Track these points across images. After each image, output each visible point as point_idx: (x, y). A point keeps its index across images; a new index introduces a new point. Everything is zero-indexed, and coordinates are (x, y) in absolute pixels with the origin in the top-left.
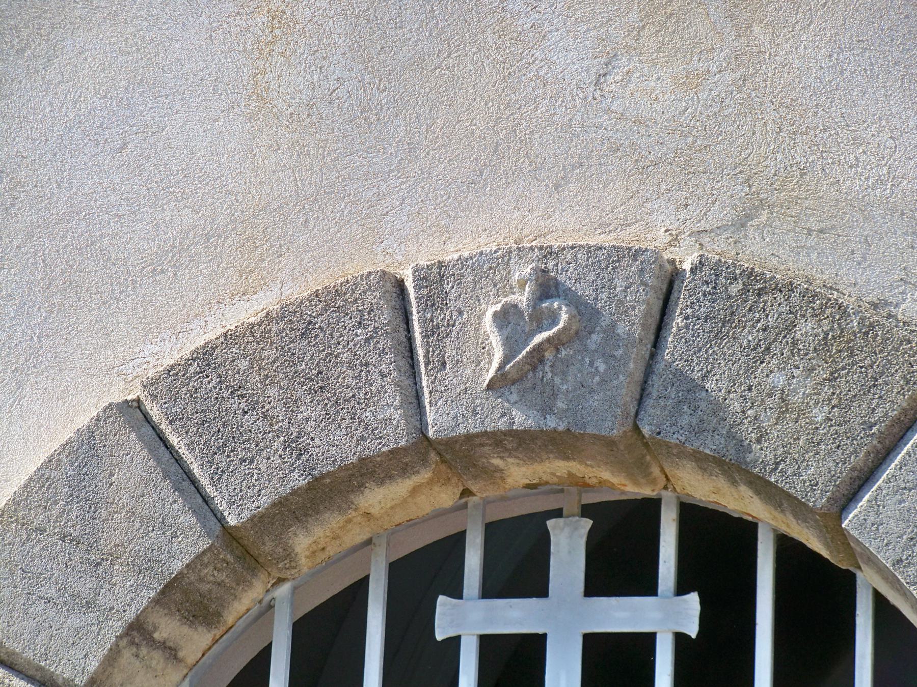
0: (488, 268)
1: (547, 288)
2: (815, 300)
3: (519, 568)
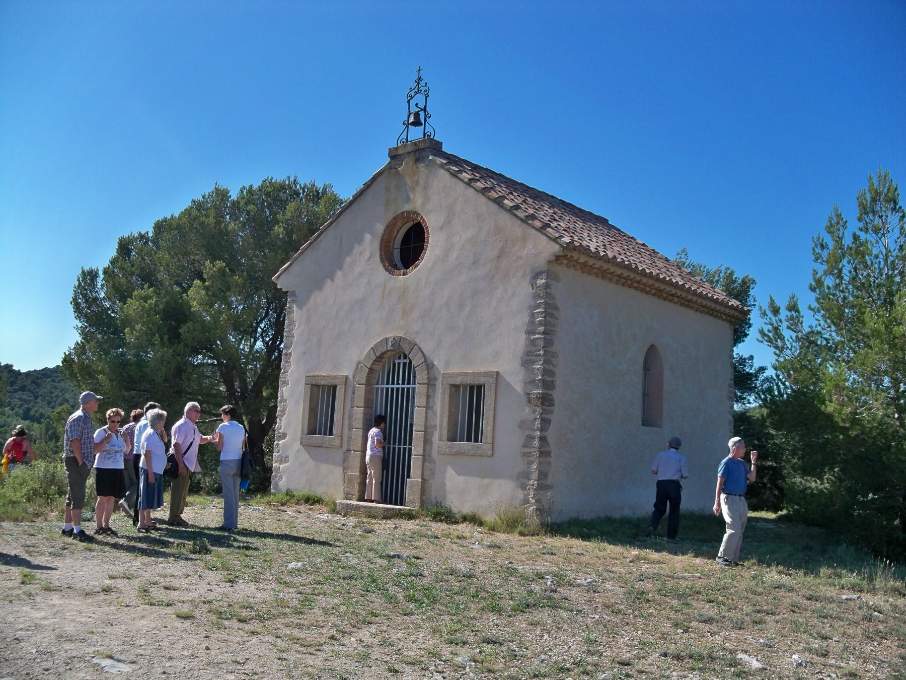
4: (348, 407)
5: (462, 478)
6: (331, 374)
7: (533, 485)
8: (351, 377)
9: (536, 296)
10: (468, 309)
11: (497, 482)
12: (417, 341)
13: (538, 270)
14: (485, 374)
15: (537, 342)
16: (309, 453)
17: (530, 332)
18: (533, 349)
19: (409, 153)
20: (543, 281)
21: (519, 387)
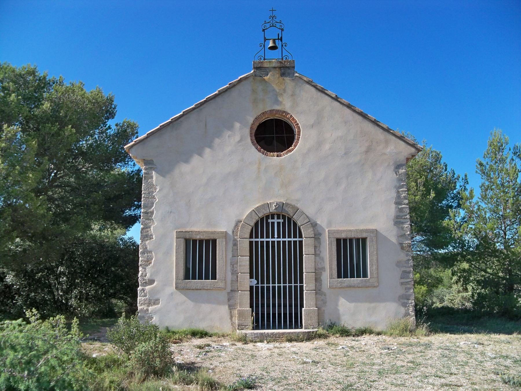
0: (273, 203)
3: (273, 218)
4: (230, 255)
6: (206, 229)
7: (411, 303)
8: (230, 233)
9: (400, 180)
10: (343, 186)
11: (382, 305)
12: (298, 205)
13: (398, 163)
14: (367, 231)
15: (404, 210)
16: (185, 295)
17: (397, 203)
18: (401, 214)
19: (275, 68)
20: (404, 170)
21: (394, 240)
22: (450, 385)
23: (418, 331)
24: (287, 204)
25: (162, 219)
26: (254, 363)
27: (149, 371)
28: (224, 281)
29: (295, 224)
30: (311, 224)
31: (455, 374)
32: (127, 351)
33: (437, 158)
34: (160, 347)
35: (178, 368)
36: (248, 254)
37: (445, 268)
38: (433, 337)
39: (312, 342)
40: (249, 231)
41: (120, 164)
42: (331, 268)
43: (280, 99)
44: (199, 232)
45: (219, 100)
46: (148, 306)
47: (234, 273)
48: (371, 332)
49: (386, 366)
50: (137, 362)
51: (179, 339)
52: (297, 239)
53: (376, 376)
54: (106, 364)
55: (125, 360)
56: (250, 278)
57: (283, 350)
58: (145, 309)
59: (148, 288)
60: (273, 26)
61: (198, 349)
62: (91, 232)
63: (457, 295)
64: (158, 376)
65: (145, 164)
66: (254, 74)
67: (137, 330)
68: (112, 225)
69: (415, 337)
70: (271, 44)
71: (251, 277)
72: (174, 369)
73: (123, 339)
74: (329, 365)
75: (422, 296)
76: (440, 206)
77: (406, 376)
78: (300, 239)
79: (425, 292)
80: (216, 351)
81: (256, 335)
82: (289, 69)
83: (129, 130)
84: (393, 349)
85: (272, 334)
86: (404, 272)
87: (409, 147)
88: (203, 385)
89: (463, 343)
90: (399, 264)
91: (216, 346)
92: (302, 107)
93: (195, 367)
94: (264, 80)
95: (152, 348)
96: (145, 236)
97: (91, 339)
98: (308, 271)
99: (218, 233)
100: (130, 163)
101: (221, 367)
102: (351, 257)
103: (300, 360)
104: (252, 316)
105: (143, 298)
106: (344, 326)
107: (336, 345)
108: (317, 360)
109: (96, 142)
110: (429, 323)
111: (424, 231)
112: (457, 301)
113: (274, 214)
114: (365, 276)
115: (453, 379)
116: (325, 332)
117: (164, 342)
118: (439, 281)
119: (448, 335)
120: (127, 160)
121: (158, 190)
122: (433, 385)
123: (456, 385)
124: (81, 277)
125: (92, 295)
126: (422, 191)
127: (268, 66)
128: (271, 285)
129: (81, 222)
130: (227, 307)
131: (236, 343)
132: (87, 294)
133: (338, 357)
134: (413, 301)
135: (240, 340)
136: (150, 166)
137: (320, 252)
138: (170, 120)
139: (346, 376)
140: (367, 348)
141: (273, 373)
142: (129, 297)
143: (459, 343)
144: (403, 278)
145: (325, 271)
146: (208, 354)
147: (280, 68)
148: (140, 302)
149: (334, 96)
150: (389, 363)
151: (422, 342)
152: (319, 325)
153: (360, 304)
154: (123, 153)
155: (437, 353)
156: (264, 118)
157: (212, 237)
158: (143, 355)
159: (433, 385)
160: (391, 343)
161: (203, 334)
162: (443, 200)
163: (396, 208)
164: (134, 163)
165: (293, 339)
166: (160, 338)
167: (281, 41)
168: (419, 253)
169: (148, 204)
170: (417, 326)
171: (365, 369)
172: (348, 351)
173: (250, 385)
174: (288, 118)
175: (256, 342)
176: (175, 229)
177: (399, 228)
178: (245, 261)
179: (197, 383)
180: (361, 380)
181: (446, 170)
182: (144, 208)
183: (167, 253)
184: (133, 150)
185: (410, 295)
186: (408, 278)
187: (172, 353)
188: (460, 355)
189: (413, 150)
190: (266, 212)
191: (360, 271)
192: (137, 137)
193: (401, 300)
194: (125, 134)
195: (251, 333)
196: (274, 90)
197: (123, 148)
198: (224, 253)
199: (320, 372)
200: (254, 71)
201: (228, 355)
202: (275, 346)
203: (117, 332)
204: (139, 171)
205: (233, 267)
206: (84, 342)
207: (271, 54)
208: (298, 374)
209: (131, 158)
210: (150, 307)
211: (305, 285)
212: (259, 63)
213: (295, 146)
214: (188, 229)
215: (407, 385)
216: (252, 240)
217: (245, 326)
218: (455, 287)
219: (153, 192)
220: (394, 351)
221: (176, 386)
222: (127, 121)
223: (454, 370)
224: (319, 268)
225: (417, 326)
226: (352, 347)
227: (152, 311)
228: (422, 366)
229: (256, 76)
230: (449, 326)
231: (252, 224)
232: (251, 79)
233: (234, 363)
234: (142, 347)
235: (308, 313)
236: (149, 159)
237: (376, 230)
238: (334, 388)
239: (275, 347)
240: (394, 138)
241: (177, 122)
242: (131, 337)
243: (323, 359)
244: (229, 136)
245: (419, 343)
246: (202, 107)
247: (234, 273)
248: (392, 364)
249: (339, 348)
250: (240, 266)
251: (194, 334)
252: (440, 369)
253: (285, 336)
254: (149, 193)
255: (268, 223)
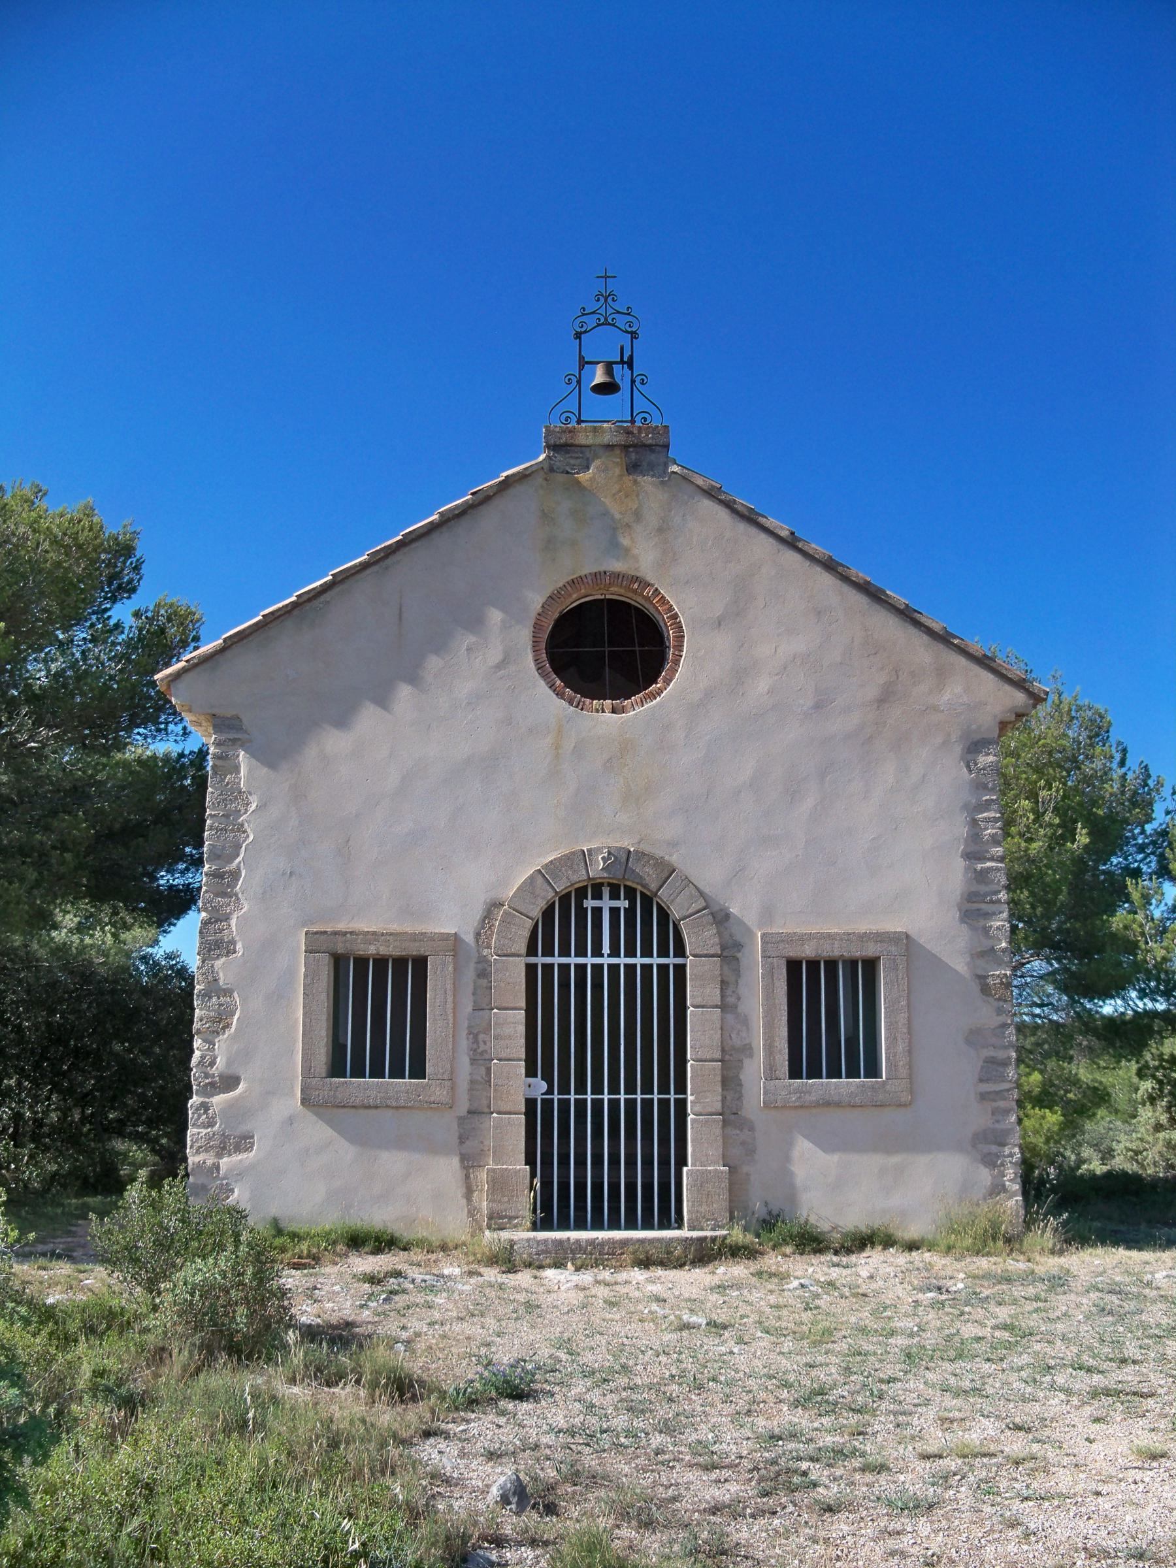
0: (599, 850)
1: (609, 853)
2: (653, 858)
3: (598, 896)
4: (467, 1007)
5: (835, 1158)
6: (394, 927)
7: (1011, 1155)
8: (469, 938)
10: (809, 803)
11: (922, 1161)
12: (674, 859)
13: (978, 737)
15: (992, 875)
16: (330, 1123)
17: (973, 856)
18: (983, 889)
19: (609, 447)
20: (991, 758)
21: (960, 965)
22: (1118, 1393)
23: (1031, 1239)
24: (641, 855)
25: (264, 893)
26: (533, 1327)
27: (216, 1345)
28: (448, 1083)
29: (664, 915)
30: (712, 914)
31: (1135, 1362)
32: (151, 1286)
33: (1098, 731)
34: (250, 1271)
35: (302, 1336)
36: (523, 1004)
37: (1118, 1058)
38: (1074, 1257)
39: (710, 1267)
40: (527, 934)
41: (141, 730)
42: (770, 1048)
43: (625, 541)
44: (374, 933)
45: (440, 540)
46: (219, 1155)
47: (480, 1058)
48: (888, 1242)
49: (930, 1339)
50: (180, 1316)
51: (308, 1256)
52: (671, 961)
53: (898, 1367)
54: (82, 1321)
55: (144, 1310)
56: (527, 1076)
57: (623, 1290)
58: (209, 1163)
59: (218, 1100)
60: (606, 323)
61: (367, 1285)
62: (54, 934)
63: (1150, 1139)
64: (239, 1359)
65: (217, 728)
66: (546, 466)
67: (183, 1221)
68: (115, 913)
69: (1022, 1257)
70: (599, 377)
71: (531, 1072)
72: (291, 1337)
73: (137, 1248)
74: (759, 1334)
75: (1047, 1141)
76: (1104, 872)
77: (987, 1367)
78: (679, 961)
79: (1056, 1128)
80: (420, 1289)
81: (542, 1247)
82: (653, 451)
83: (172, 630)
84: (954, 1289)
85: (592, 1242)
86: (991, 1061)
87: (1007, 688)
88: (377, 1385)
89: (1165, 1273)
90: (974, 1037)
91: (419, 1278)
92: (687, 562)
93: (354, 1336)
94: (578, 482)
95: (224, 1274)
96: (214, 945)
97: (44, 1255)
98: (700, 1055)
99: (432, 938)
100: (171, 727)
101: (431, 1337)
102: (831, 1010)
103: (672, 1317)
104: (531, 1188)
105: (204, 1131)
106: (807, 1222)
107: (783, 1277)
108: (722, 1317)
109: (74, 665)
110: (1065, 1215)
111: (1055, 947)
112: (1151, 1155)
113: (602, 884)
114: (873, 1071)
115: (1128, 1374)
116: (750, 1238)
117: (262, 1260)
118: (1100, 1096)
119: (1122, 1253)
120: (162, 719)
121: (254, 806)
122: (1068, 1392)
123: (1135, 1394)
124: (21, 1071)
125: (52, 1125)
126: (1050, 825)
127: (590, 441)
128: (589, 1097)
129: (18, 903)
130: (455, 1161)
131: (482, 1270)
132: (39, 1124)
133: (785, 1312)
134: (1017, 1150)
135: (493, 1260)
136: (231, 736)
137: (739, 999)
138: (294, 599)
139: (806, 1365)
140: (874, 1286)
141: (588, 1354)
142: (166, 1135)
143: (1152, 1273)
144: (987, 1080)
145: (751, 1056)
146: (396, 1298)
147: (625, 448)
148: (193, 1143)
149: (784, 533)
150: (940, 1329)
151: (1040, 1270)
152: (732, 1218)
153: (854, 1157)
154: (151, 698)
155: (1084, 1301)
156: (575, 596)
157: (414, 949)
158: (197, 1297)
159: (1068, 1392)
160: (949, 1273)
161: (383, 1243)
162: (1114, 854)
163: (967, 869)
164: (185, 728)
165: (654, 1258)
166: (249, 1244)
167: (631, 367)
168: (1037, 1011)
169: (224, 848)
170: (1028, 1224)
171: (866, 1347)
172: (817, 1296)
173: (517, 1387)
174: (647, 599)
175: (541, 1267)
176: (303, 925)
177: (973, 929)
178: (512, 1024)
179: (358, 1382)
180: (853, 1378)
181: (1122, 763)
182: (210, 860)
183: (279, 997)
184: (182, 685)
185: (1008, 1132)
186: (1003, 1078)
187: (283, 1293)
188: (1154, 1308)
189: (1020, 698)
190: (578, 877)
191: (860, 1059)
192: (196, 648)
193: (980, 1146)
194: (159, 641)
195: (528, 1240)
196: (606, 513)
197: (153, 684)
198: (450, 999)
199: (732, 1353)
200: (548, 457)
201: (456, 1302)
202: (600, 1278)
203: (122, 1227)
204: (202, 754)
205: (476, 1041)
206: (22, 1263)
207: (598, 406)
208: (663, 1358)
209: (175, 713)
210: (225, 1159)
211: (690, 1098)
212: (564, 431)
213: (667, 682)
214: (341, 926)
215: (990, 1391)
216: (532, 960)
217: (511, 1218)
218: (1146, 1114)
219: (238, 813)
220: (957, 1296)
221: (295, 1390)
222: (169, 601)
223: (1131, 1351)
224: (733, 1048)
225: (1028, 1224)
226: (831, 1284)
227: (230, 1170)
228: (1038, 1338)
229: (552, 470)
230: (1123, 1228)
231: (536, 912)
232: (539, 480)
233: (473, 1324)
234: (196, 1271)
235: (701, 1180)
236: (230, 713)
237: (907, 936)
238: (771, 1399)
239: (598, 1282)
240: (963, 661)
241: (316, 603)
242: (164, 1243)
243: (742, 1317)
244: (469, 650)
245: (1033, 1272)
246: (389, 561)
247: (480, 1058)
248: (947, 1332)
249: (791, 1286)
250: (497, 1037)
251: (357, 1241)
252: (1090, 1348)
253: (631, 1249)
254: (226, 816)
255: (581, 912)
